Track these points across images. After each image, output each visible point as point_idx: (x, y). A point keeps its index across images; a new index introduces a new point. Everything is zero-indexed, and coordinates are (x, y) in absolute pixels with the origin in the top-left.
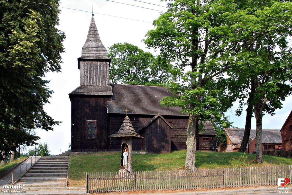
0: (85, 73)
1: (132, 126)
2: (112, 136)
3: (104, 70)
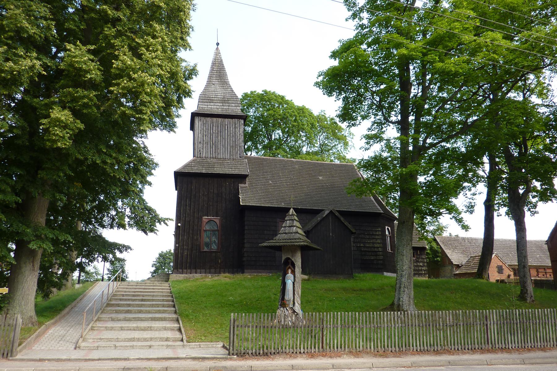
0: (203, 136)
1: (301, 227)
2: (265, 244)
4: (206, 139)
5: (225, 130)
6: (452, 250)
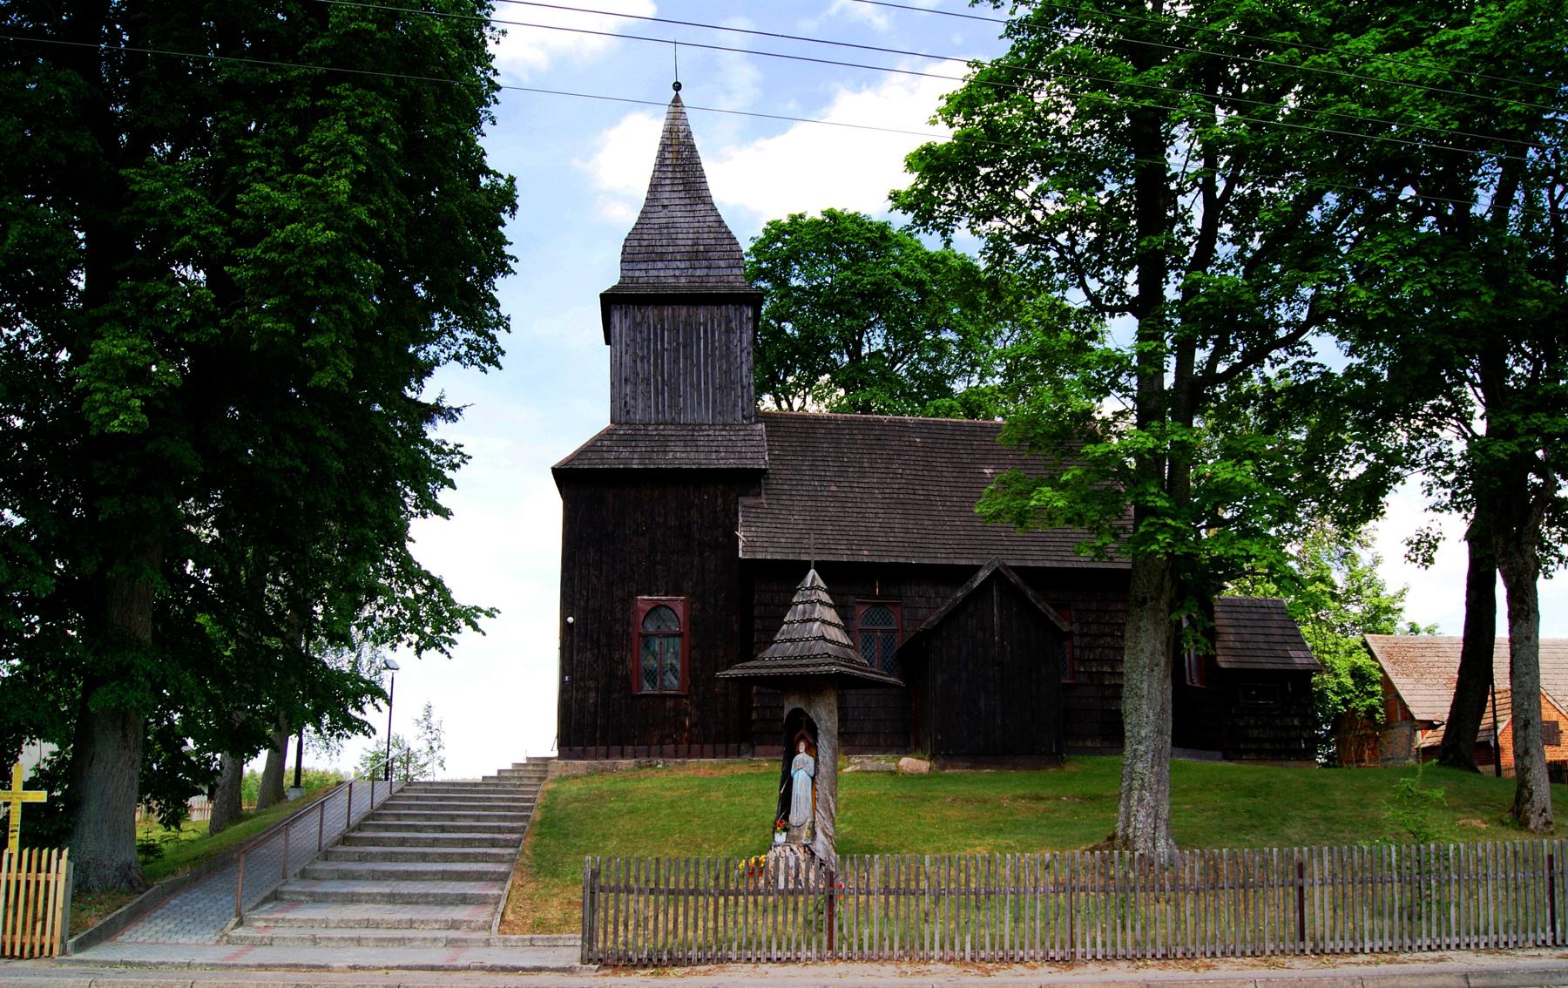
0: (635, 361)
1: (837, 620)
2: (736, 672)
3: (728, 348)
4: (643, 368)
5: (699, 338)
6: (1415, 675)
